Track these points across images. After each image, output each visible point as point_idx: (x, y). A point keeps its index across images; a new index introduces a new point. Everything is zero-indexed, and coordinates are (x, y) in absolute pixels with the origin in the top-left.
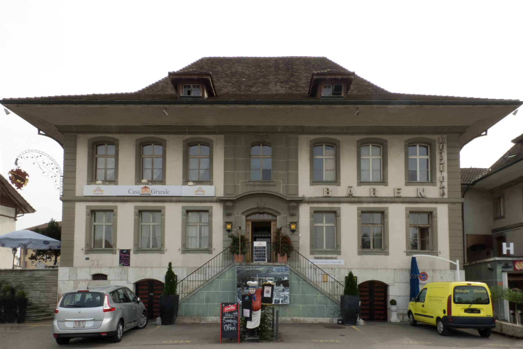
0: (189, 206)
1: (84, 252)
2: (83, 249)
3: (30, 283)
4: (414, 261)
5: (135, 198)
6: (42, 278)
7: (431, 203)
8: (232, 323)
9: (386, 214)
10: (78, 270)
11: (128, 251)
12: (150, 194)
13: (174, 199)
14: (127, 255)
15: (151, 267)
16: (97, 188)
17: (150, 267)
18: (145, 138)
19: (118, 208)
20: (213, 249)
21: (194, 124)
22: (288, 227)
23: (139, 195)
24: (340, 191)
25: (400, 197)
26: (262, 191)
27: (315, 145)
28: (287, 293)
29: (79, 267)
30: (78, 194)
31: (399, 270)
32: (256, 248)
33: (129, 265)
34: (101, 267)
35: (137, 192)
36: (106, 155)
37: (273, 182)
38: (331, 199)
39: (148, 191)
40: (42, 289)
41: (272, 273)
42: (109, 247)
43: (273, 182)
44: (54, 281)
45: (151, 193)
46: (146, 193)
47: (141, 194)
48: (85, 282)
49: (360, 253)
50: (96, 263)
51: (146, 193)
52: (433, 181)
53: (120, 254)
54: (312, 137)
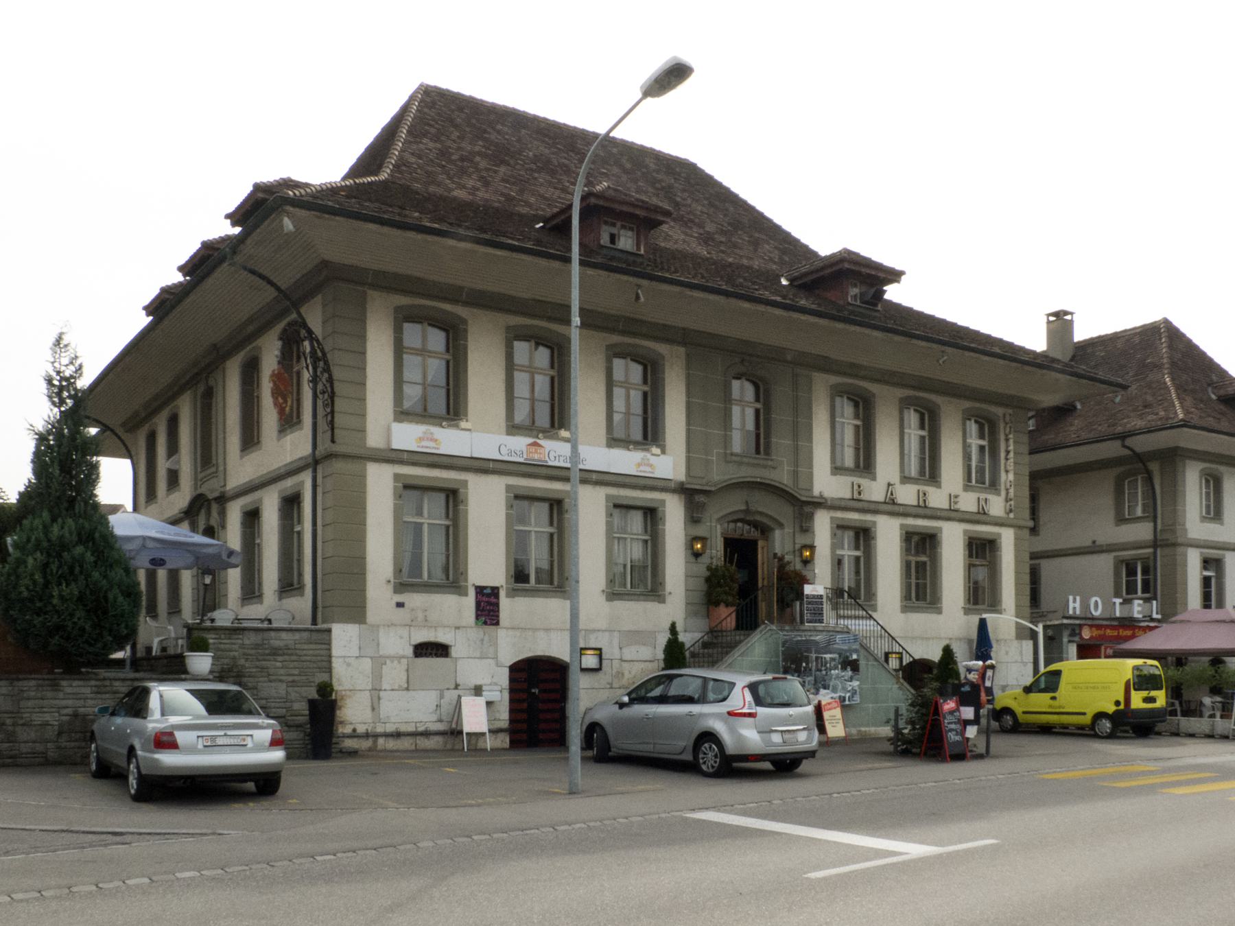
0: (619, 496)
1: (390, 587)
2: (389, 581)
3: (259, 661)
4: (983, 625)
5: (511, 467)
6: (289, 649)
7: (996, 524)
8: (956, 730)
9: (566, 506)
10: (382, 630)
11: (496, 591)
12: (547, 462)
13: (594, 476)
14: (493, 600)
15: (547, 630)
16: (425, 433)
17: (544, 629)
18: (526, 326)
19: (470, 484)
20: (667, 594)
21: (644, 318)
22: (797, 553)
23: (521, 460)
24: (875, 491)
25: (956, 511)
26: (761, 478)
27: (404, 317)
28: (856, 683)
29: (384, 625)
30: (374, 440)
31: (956, 639)
32: (808, 596)
33: (497, 624)
34: (435, 627)
35: (518, 453)
36: (334, 332)
37: (772, 460)
38: (866, 505)
39: (540, 453)
40: (291, 678)
41: (835, 646)
42: (452, 580)
43: (772, 460)
44: (319, 658)
45: (547, 459)
46: (536, 457)
47: (526, 459)
48: (399, 662)
49: (905, 609)
50: (420, 616)
51: (536, 456)
52: (774, 457)
53: (477, 597)
54: (404, 300)
